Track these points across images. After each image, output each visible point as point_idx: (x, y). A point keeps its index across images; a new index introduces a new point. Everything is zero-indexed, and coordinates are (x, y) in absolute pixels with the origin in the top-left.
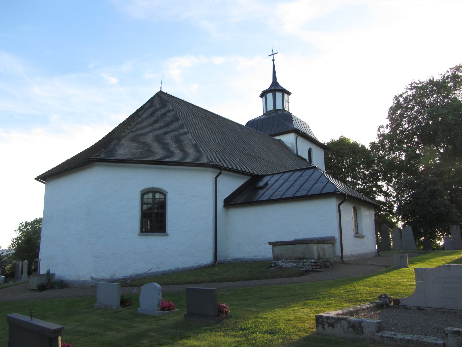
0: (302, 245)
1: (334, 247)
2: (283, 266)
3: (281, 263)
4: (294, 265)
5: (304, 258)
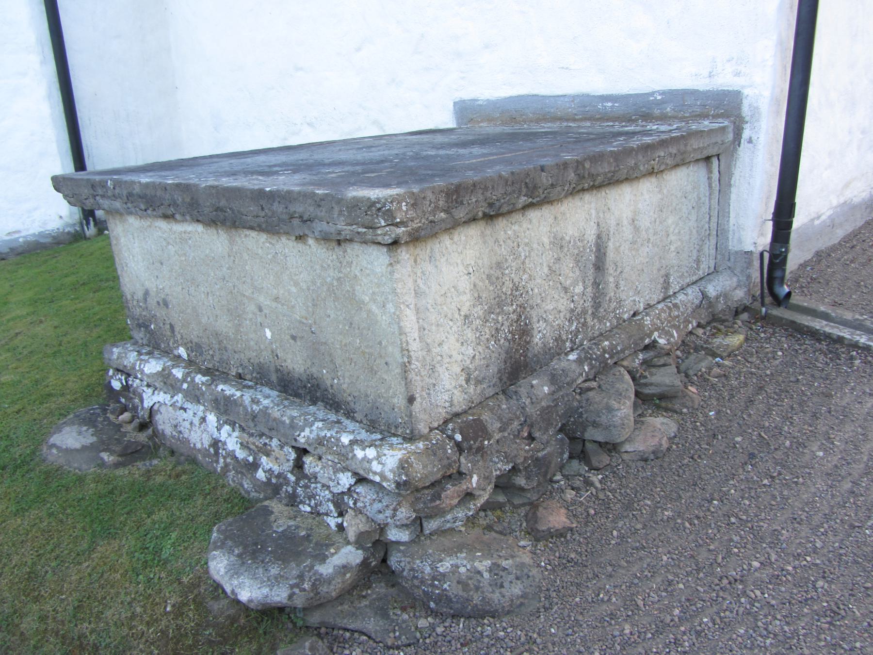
1: (723, 187)
4: (231, 440)
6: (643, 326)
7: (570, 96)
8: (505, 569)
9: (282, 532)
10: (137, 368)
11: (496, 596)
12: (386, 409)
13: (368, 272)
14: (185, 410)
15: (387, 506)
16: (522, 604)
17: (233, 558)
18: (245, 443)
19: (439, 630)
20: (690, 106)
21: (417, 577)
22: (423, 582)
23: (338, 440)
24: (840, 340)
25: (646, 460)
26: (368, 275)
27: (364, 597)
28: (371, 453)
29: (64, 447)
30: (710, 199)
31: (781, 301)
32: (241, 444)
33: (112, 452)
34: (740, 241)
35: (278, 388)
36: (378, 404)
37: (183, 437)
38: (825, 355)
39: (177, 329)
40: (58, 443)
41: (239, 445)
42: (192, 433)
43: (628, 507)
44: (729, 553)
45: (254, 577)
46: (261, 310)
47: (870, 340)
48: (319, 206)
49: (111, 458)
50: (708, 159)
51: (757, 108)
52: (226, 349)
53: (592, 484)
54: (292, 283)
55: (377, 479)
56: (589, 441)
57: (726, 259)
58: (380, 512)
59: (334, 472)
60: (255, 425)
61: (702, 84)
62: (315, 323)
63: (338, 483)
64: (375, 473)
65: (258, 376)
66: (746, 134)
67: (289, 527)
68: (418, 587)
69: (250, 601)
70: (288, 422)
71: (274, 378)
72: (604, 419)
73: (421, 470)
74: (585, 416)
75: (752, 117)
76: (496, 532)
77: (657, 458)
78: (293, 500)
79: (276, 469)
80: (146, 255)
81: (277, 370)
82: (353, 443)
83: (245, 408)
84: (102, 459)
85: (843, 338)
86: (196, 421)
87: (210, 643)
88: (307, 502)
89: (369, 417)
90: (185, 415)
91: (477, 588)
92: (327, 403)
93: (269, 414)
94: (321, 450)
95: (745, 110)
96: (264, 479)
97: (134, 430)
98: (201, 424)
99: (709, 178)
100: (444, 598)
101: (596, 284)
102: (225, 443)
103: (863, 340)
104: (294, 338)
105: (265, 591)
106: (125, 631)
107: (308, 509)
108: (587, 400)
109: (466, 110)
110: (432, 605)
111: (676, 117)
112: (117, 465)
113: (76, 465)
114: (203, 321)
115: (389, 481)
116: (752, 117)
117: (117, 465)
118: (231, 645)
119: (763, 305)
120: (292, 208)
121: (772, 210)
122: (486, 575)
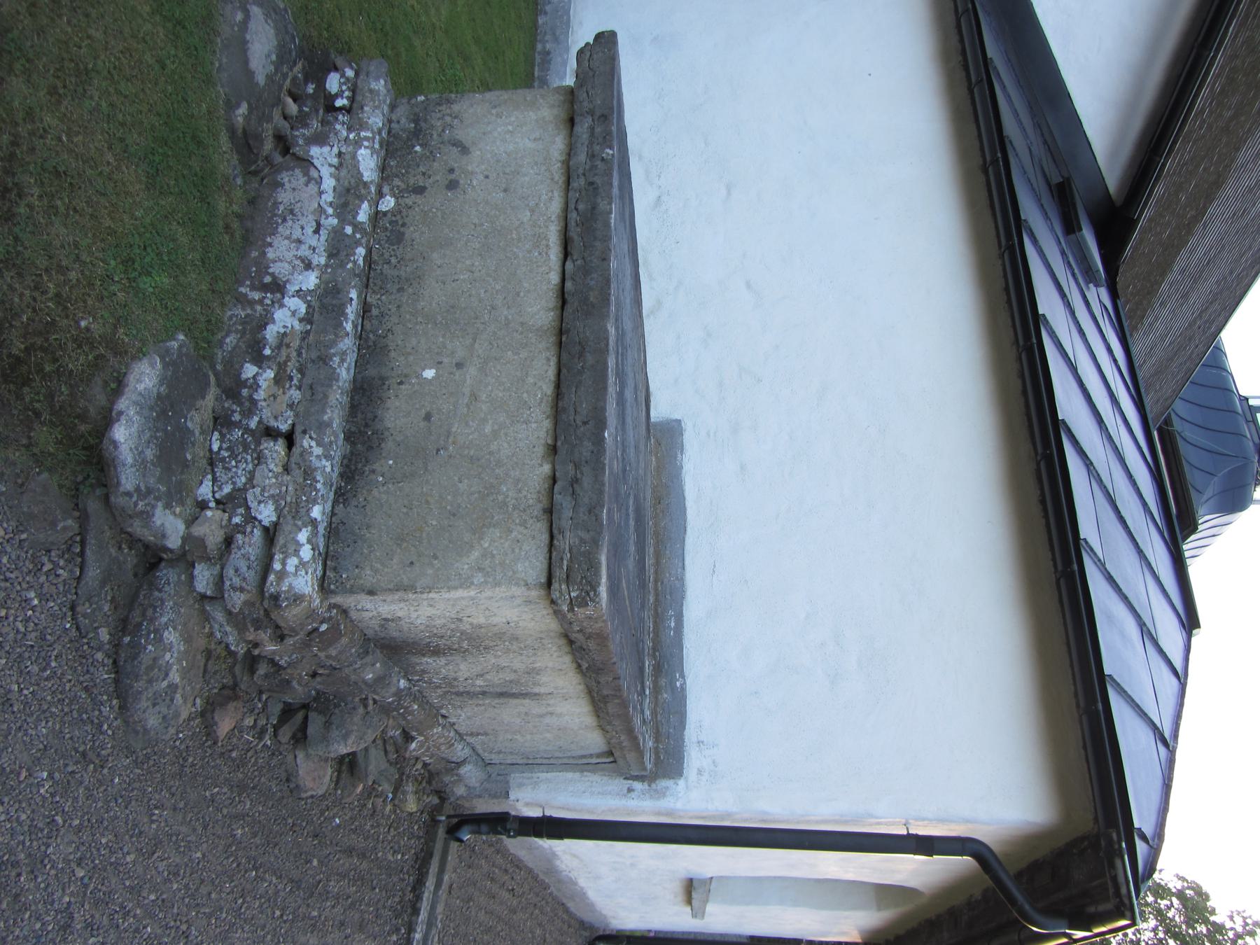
0: (537, 428)
1: (582, 764)
2: (292, 180)
3: (345, 163)
4: (286, 317)
5: (363, 438)
6: (432, 727)
7: (683, 574)
8: (172, 700)
9: (187, 428)
10: (363, 134)
11: (144, 704)
12: (356, 555)
13: (517, 551)
14: (317, 231)
15: (245, 579)
16: (137, 733)
17: (155, 390)
18: (286, 340)
19: (99, 656)
20: (668, 721)
21: (155, 611)
22: (152, 620)
23: (315, 502)
24: (416, 911)
25: (288, 780)
26: (513, 551)
27: (120, 548)
28: (306, 553)
29: (248, 37)
30: (569, 757)
31: (453, 831)
32: (285, 334)
33: (247, 118)
34: (521, 785)
35: (359, 377)
36: (360, 543)
37: (277, 224)
38: (400, 902)
39: (419, 199)
40: (252, 25)
41: (282, 331)
42: (286, 242)
43: (242, 788)
44: (209, 916)
45: (140, 433)
46: (459, 365)
47: (418, 942)
48: (590, 512)
49: (240, 119)
50: (610, 753)
51: (664, 795)
52: (401, 290)
53: (261, 739)
54: (496, 427)
55: (277, 566)
56: (306, 718)
57: (499, 776)
58: (236, 571)
59: (273, 496)
60: (313, 361)
61: (691, 733)
62: (450, 457)
63: (260, 502)
64: (284, 564)
65: (371, 343)
66: (638, 785)
67: (193, 433)
68: (144, 615)
69: (115, 444)
70: (326, 418)
71: (372, 372)
72: (335, 733)
73: (290, 615)
74: (337, 711)
75: (656, 790)
76: (205, 665)
77: (291, 792)
78: (221, 422)
79: (260, 395)
80: (510, 140)
81: (383, 379)
82: (314, 523)
83: (334, 343)
84: (238, 105)
85: (418, 915)
86: (304, 251)
87: (50, 396)
88: (225, 446)
89: (341, 528)
90: (309, 230)
91: (150, 681)
92: (350, 460)
93: (331, 386)
94: (297, 473)
95: (663, 783)
96: (244, 376)
97: (276, 128)
98: (302, 260)
99: (591, 756)
100: (136, 649)
101: (484, 693)
102: (282, 306)
103: (418, 936)
104: (428, 417)
105: (130, 460)
106: (42, 262)
107: (215, 447)
108: (354, 708)
109: (666, 439)
110: (127, 639)
111: (656, 704)
112: (232, 131)
113: (225, 60)
114: (435, 255)
115: (278, 584)
116: (656, 790)
117: (232, 131)
118: (51, 421)
119: (449, 817)
120: (586, 469)
121: (555, 815)
122: (165, 684)
